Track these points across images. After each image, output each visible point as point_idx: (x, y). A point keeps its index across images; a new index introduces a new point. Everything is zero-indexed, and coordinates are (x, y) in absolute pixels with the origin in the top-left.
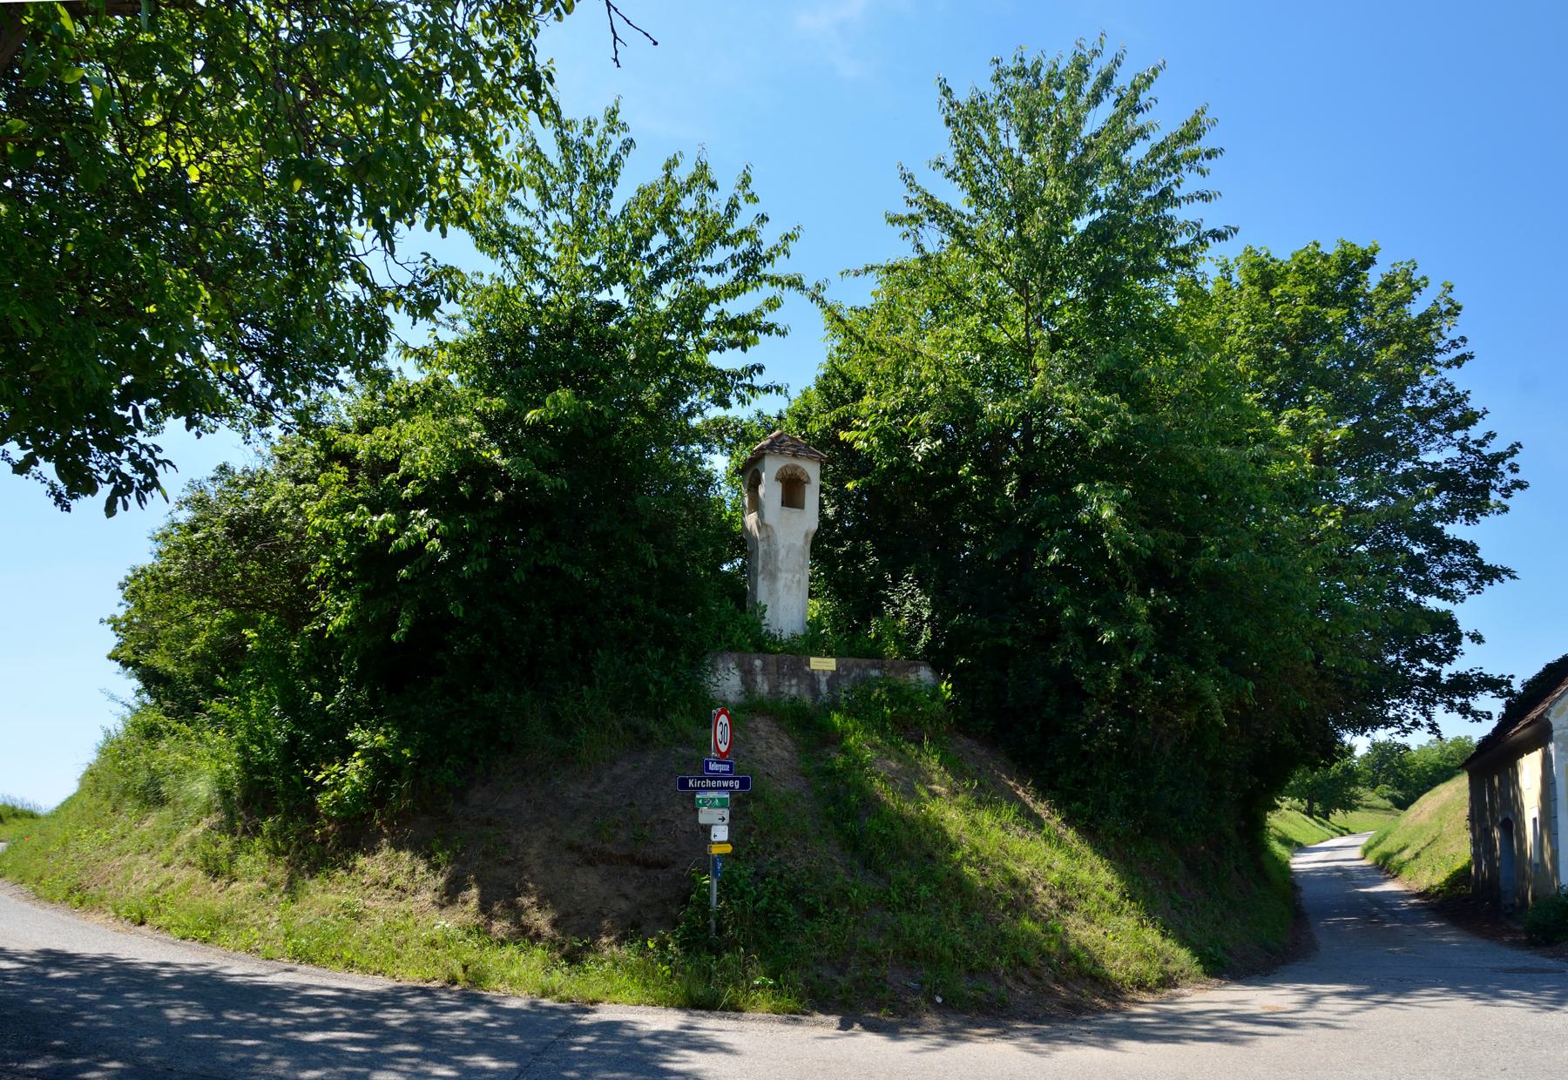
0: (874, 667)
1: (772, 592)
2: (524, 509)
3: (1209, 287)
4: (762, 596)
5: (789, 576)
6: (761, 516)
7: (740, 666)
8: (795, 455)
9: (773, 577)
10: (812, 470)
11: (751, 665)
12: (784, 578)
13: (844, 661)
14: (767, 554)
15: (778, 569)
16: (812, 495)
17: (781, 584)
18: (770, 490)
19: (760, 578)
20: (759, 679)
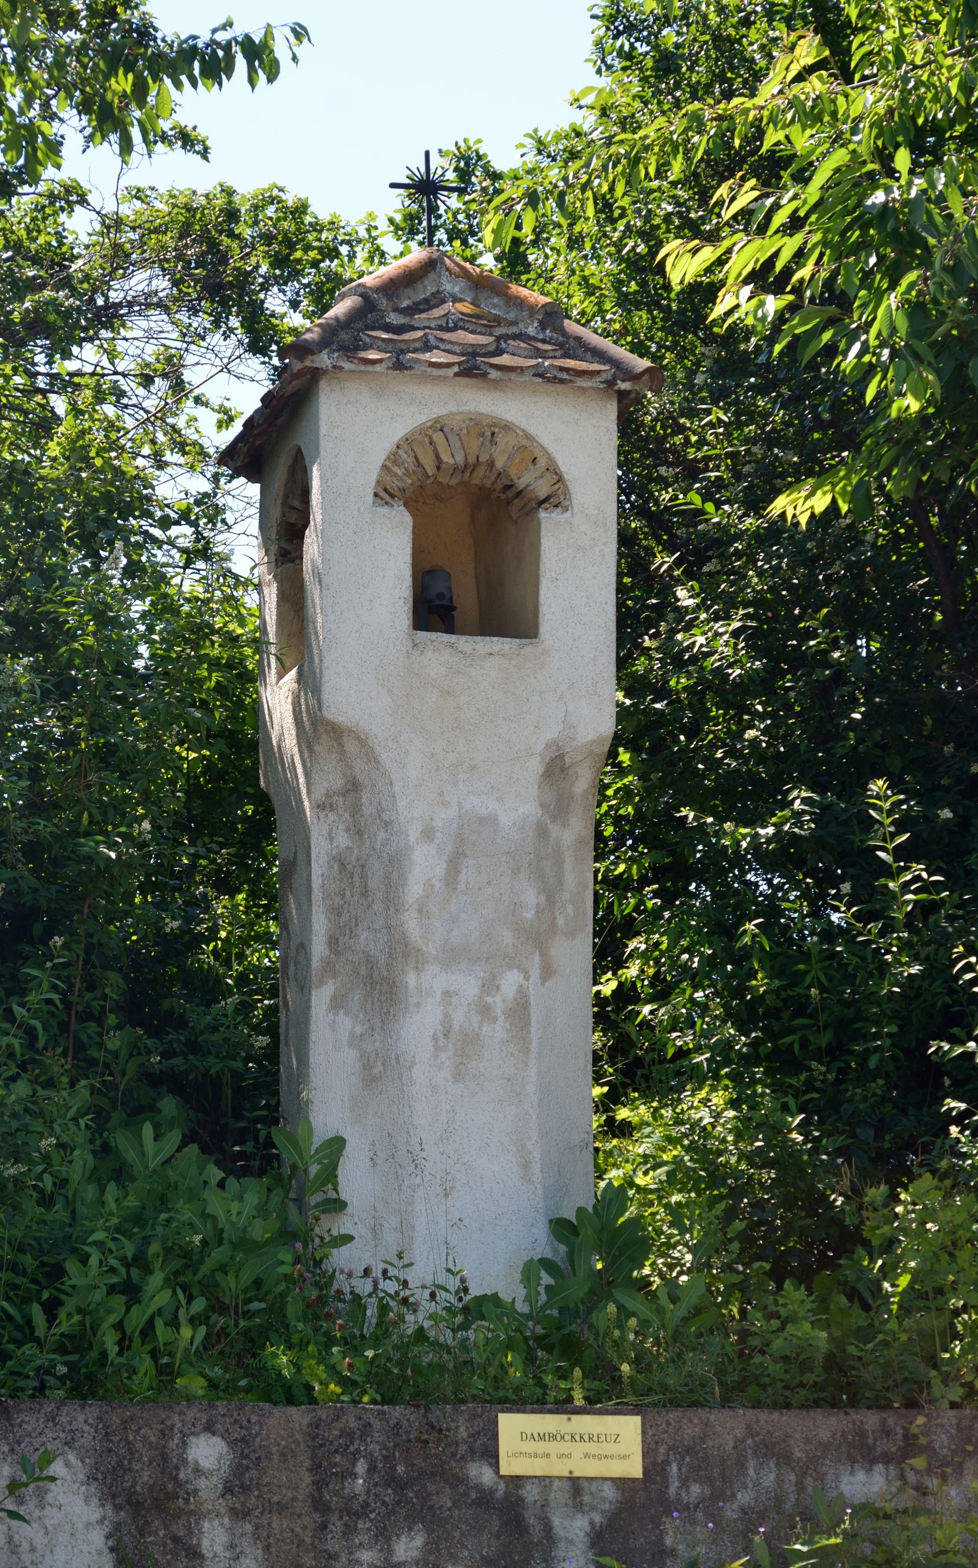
0: (862, 1453)
1: (379, 1071)
3: (49, 173)
5: (467, 985)
6: (309, 683)
7: (110, 1481)
8: (471, 368)
9: (381, 991)
10: (579, 445)
11: (169, 1465)
12: (436, 996)
13: (689, 1425)
14: (559, 809)
15: (402, 950)
16: (577, 569)
17: (419, 1027)
18: (366, 558)
19: (321, 999)
20: (214, 1537)
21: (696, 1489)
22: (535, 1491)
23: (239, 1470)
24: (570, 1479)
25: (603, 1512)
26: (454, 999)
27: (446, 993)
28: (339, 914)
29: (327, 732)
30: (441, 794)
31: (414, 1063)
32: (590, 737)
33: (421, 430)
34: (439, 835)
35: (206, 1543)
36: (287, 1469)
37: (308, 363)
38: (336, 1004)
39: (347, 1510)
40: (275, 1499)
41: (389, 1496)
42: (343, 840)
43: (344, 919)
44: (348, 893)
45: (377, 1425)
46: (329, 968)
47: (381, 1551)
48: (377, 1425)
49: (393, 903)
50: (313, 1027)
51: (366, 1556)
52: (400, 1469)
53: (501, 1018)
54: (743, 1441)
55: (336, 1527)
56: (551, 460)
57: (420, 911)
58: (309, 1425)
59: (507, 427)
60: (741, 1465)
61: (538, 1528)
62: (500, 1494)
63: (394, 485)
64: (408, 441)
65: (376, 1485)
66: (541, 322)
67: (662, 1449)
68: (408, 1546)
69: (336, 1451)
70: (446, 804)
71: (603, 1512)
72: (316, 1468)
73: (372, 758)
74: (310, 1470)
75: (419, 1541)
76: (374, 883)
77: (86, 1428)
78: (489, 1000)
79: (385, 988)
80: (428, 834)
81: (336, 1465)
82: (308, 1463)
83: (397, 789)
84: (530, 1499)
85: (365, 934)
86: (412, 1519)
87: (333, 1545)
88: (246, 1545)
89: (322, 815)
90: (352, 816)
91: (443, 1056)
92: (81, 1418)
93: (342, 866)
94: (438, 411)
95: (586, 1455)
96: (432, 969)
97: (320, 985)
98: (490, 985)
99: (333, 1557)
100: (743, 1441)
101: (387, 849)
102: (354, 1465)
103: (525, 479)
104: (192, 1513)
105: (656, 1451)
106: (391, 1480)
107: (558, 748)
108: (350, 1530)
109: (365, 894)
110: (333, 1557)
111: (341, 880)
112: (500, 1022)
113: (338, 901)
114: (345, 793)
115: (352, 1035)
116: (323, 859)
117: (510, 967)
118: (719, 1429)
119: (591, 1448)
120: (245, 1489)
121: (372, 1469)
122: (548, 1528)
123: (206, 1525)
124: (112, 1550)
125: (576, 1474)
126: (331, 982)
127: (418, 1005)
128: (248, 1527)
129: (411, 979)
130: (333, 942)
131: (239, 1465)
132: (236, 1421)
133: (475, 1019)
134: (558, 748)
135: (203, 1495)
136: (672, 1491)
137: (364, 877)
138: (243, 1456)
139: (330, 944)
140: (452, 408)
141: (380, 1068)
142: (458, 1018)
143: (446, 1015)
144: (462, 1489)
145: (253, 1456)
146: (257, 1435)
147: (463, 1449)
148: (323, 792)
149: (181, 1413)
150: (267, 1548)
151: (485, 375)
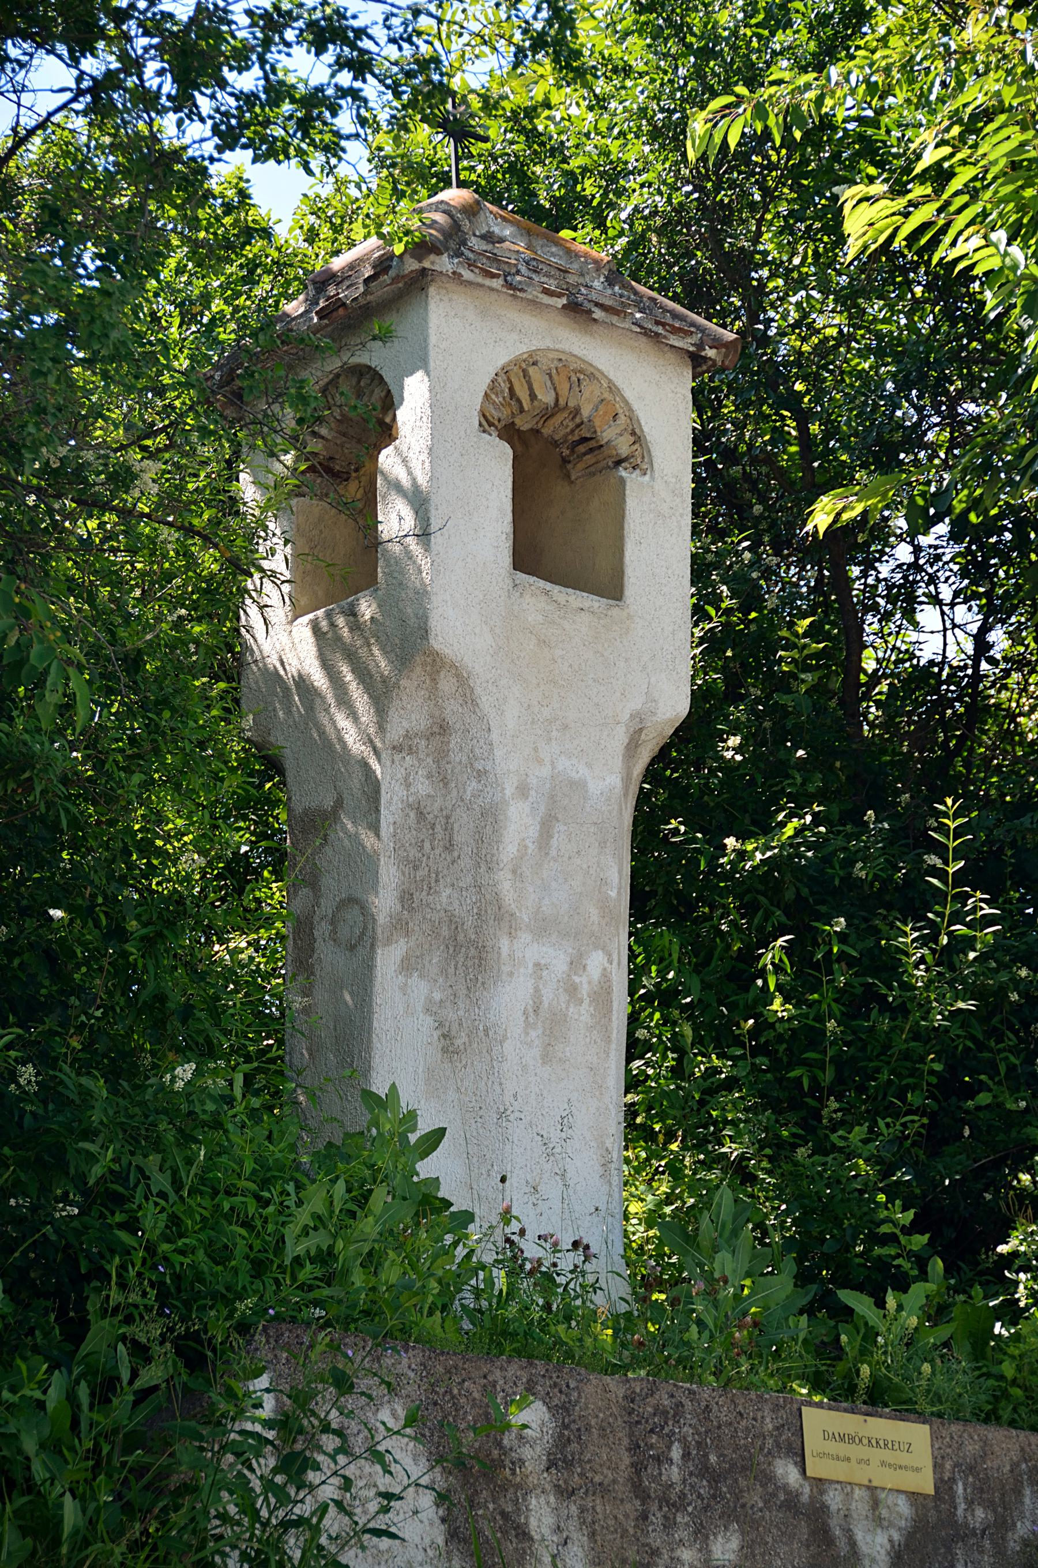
2: (712, 737)
4: (401, 1059)
9: (467, 955)
11: (494, 1425)
15: (491, 912)
16: (658, 523)
17: (510, 999)
19: (388, 960)
20: (541, 1515)
21: (980, 1513)
22: (838, 1499)
23: (561, 1442)
24: (868, 1488)
25: (900, 1529)
26: (545, 973)
27: (537, 965)
28: (416, 868)
29: (424, 664)
30: (536, 749)
31: (505, 1037)
32: (668, 715)
33: (516, 362)
34: (533, 793)
35: (533, 1523)
36: (607, 1445)
37: (426, 264)
38: (407, 966)
39: (664, 1500)
40: (597, 1479)
41: (704, 1487)
42: (422, 787)
43: (420, 873)
44: (427, 845)
45: (688, 1404)
46: (400, 926)
47: (700, 1550)
48: (688, 1404)
49: (484, 858)
50: (378, 987)
51: (687, 1555)
52: (713, 1458)
53: (587, 1002)
54: (1017, 1465)
55: (657, 1518)
56: (632, 417)
57: (514, 872)
58: (625, 1397)
59: (592, 375)
60: (1019, 1493)
61: (844, 1540)
62: (805, 1498)
63: (494, 413)
64: (506, 371)
65: (691, 1474)
66: (607, 278)
67: (948, 1465)
68: (726, 1546)
69: (652, 1431)
70: (540, 761)
71: (900, 1529)
72: (634, 1448)
73: (468, 697)
74: (629, 1450)
75: (735, 1544)
76: (462, 836)
77: (412, 1375)
78: (577, 979)
79: (472, 952)
80: (523, 791)
81: (652, 1447)
82: (626, 1442)
83: (494, 736)
84: (833, 1508)
85: (448, 891)
86: (730, 1516)
87: (656, 1539)
88: (572, 1528)
89: (397, 757)
90: (437, 762)
91: (533, 1034)
92: (405, 1361)
93: (421, 815)
94: (536, 344)
95: (883, 1464)
96: (525, 937)
97: (389, 942)
98: (577, 964)
99: (655, 1553)
100: (1017, 1465)
101: (480, 801)
102: (669, 1448)
103: (607, 434)
104: (518, 1487)
105: (942, 1466)
106: (704, 1470)
107: (641, 721)
108: (669, 1525)
109: (449, 847)
110: (655, 1553)
111: (419, 830)
112: (585, 1004)
113: (413, 853)
114: (430, 736)
115: (429, 1000)
116: (397, 805)
117: (596, 947)
118: (996, 1449)
119: (887, 1455)
120: (569, 1464)
121: (686, 1455)
122: (853, 1543)
123: (534, 1501)
124: (443, 1520)
125: (874, 1484)
126: (402, 941)
127: (511, 974)
128: (574, 1509)
129: (504, 944)
130: (406, 898)
131: (561, 1435)
132: (555, 1385)
133: (563, 998)
134: (641, 721)
135: (529, 1466)
136: (960, 1512)
137: (448, 828)
138: (566, 1427)
139: (402, 900)
140: (548, 343)
141: (465, 1039)
142: (548, 995)
143: (537, 990)
144: (771, 1488)
145: (574, 1427)
146: (577, 1402)
147: (770, 1442)
148: (402, 732)
149: (502, 1368)
150: (592, 1535)
151: (590, 312)
